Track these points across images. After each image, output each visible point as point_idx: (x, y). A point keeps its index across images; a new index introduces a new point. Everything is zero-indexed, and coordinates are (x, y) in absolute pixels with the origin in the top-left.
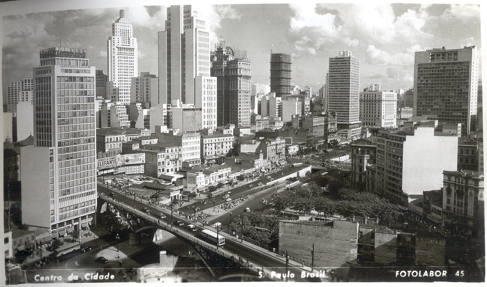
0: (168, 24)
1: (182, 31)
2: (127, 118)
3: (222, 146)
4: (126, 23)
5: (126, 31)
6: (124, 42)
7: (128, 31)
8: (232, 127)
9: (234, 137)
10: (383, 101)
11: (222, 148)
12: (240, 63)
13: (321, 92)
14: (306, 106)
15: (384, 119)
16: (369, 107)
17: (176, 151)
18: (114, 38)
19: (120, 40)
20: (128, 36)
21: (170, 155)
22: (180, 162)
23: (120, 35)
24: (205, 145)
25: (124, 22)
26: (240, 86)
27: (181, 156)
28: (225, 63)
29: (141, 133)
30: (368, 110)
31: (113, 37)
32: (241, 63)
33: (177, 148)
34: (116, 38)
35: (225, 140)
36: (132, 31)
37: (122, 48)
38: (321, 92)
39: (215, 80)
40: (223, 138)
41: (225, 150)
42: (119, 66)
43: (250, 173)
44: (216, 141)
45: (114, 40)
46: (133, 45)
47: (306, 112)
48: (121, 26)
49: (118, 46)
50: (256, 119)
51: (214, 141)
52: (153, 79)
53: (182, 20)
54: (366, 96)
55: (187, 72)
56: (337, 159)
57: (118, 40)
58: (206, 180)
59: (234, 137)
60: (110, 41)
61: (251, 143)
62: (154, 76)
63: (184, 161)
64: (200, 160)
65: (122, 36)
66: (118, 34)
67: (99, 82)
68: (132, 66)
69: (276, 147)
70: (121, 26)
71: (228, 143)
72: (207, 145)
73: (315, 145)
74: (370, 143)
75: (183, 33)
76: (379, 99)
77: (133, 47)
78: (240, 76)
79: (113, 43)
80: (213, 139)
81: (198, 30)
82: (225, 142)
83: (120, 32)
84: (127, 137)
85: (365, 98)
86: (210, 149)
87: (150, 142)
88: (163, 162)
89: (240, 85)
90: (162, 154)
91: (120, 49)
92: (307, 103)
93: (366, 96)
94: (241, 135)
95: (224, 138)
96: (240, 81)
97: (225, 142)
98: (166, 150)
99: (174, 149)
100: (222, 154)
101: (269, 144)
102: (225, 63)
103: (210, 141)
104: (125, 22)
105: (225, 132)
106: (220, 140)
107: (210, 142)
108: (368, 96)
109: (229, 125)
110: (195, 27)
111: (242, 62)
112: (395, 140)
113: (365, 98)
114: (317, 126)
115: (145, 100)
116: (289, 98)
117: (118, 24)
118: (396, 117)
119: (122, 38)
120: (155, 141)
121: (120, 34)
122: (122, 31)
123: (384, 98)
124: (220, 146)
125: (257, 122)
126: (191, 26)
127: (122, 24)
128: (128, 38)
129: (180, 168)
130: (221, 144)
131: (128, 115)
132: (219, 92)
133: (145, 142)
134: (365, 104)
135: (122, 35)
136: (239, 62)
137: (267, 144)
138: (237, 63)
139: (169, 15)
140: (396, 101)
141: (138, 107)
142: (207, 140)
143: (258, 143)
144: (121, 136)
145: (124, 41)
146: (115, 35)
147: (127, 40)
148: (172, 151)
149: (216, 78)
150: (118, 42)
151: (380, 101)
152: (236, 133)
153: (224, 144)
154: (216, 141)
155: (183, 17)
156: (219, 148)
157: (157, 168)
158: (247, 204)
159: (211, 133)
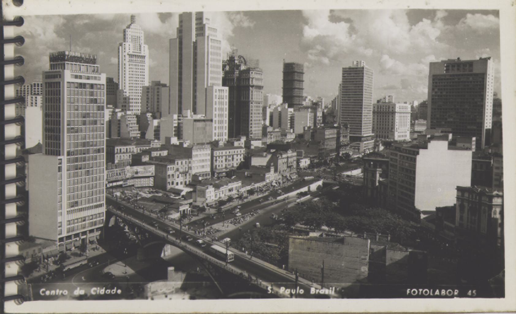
0: (180, 31)
1: (194, 39)
3: (233, 159)
6: (135, 49)
7: (140, 37)
8: (243, 139)
10: (396, 114)
12: (252, 73)
14: (318, 117)
16: (382, 119)
17: (186, 163)
18: (125, 45)
20: (140, 43)
21: (180, 168)
28: (237, 72)
30: (382, 122)
31: (124, 43)
32: (254, 72)
33: (187, 161)
34: (127, 44)
39: (226, 90)
47: (318, 124)
49: (129, 53)
51: (224, 154)
52: (163, 89)
55: (199, 82)
56: (349, 173)
60: (120, 47)
61: (262, 156)
62: (165, 86)
64: (210, 173)
68: (143, 74)
71: (239, 156)
74: (383, 156)
76: (393, 110)
78: (252, 86)
79: (124, 50)
80: (224, 152)
81: (210, 37)
83: (131, 38)
85: (378, 110)
90: (172, 166)
91: (131, 56)
92: (319, 114)
96: (252, 91)
98: (176, 162)
99: (184, 162)
101: (280, 157)
102: (237, 73)
105: (236, 144)
107: (221, 154)
110: (207, 34)
113: (378, 110)
119: (133, 45)
121: (131, 41)
123: (397, 110)
124: (231, 158)
127: (133, 30)
128: (140, 45)
129: (189, 181)
130: (232, 156)
131: (138, 126)
133: (155, 154)
134: (378, 116)
136: (251, 72)
137: (279, 157)
138: (249, 73)
139: (181, 22)
140: (410, 114)
143: (269, 156)
150: (129, 49)
151: (394, 113)
152: (248, 145)
153: (235, 156)
156: (229, 161)
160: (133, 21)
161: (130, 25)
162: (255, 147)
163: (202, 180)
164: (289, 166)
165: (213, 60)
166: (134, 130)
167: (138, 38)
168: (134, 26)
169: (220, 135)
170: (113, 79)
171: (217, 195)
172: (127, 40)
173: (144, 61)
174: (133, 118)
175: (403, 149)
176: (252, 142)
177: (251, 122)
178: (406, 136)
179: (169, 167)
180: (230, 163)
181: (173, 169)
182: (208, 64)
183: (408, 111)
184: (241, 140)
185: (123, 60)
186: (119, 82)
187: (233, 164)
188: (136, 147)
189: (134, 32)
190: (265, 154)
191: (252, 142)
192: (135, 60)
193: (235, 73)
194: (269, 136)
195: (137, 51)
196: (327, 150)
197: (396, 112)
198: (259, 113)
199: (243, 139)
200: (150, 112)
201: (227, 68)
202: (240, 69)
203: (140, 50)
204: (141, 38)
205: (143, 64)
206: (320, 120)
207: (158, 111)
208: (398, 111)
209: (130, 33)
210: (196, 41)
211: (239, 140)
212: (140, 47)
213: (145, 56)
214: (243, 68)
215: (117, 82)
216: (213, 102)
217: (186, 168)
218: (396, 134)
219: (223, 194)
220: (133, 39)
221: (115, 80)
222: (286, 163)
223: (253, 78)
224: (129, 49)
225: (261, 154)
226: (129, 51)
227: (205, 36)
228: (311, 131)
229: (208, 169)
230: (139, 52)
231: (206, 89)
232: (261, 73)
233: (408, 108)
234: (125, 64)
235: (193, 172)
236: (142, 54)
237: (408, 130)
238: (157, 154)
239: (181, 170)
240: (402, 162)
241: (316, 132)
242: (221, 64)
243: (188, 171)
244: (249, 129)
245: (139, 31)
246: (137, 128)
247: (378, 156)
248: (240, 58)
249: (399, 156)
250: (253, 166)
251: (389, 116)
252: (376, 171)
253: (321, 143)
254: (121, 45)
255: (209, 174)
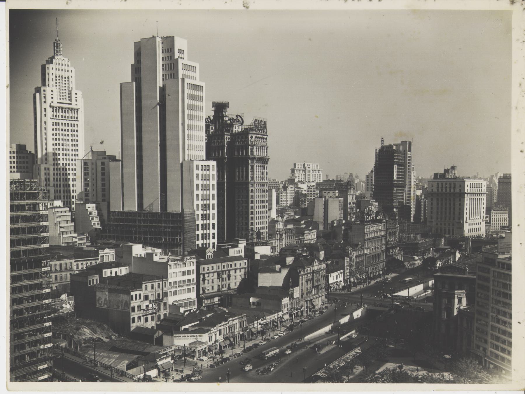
0: (137, 70)
1: (160, 83)
2: (73, 229)
3: (229, 276)
4: (65, 65)
5: (65, 78)
6: (61, 97)
7: (68, 78)
8: (242, 245)
9: (246, 261)
10: (466, 195)
11: (229, 279)
12: (252, 137)
13: (370, 179)
14: (350, 204)
15: (468, 224)
17: (159, 287)
18: (44, 91)
19: (55, 93)
20: (69, 87)
21: (150, 295)
22: (165, 304)
23: (54, 86)
24: (202, 276)
25: (60, 62)
26: (251, 174)
27: (167, 296)
28: (227, 136)
29: (100, 255)
31: (43, 88)
32: (254, 136)
33: (161, 283)
34: (48, 89)
35: (233, 267)
36: (74, 79)
37: (59, 108)
38: (370, 179)
39: (213, 166)
40: (230, 263)
41: (235, 281)
42: (53, 139)
43: (274, 319)
44: (219, 268)
45: (44, 93)
46: (76, 103)
47: (350, 214)
48: (56, 69)
49: (52, 104)
50: (276, 228)
51: (215, 269)
52: (112, 164)
53: (159, 63)
54: (440, 186)
55: (169, 154)
56: (404, 293)
57: (52, 93)
58: (211, 335)
59: (246, 261)
60: (38, 95)
61: (274, 271)
62: (113, 158)
63: (171, 304)
64: (196, 300)
65: (58, 87)
66: (51, 83)
67: (24, 165)
68: (76, 138)
69: (313, 276)
70: (56, 69)
71: (238, 271)
72: (206, 276)
73: (367, 269)
74: (462, 271)
75: (161, 86)
76: (460, 190)
77: (76, 107)
78: (253, 159)
79: (43, 100)
80: (215, 266)
81: (187, 81)
82: (233, 270)
83: (54, 80)
84: (76, 263)
85: (438, 190)
86: (211, 281)
87: (116, 273)
88: (139, 307)
89: (252, 174)
90: (138, 293)
91: (55, 109)
92: (352, 199)
93: (440, 186)
94: (257, 257)
95: (231, 263)
96: (252, 167)
97: (233, 270)
98: (144, 285)
99: (156, 285)
100: (229, 288)
101: (302, 273)
102: (228, 137)
103: (210, 269)
104: (63, 63)
105: (232, 252)
106: (225, 267)
107: (211, 270)
108: (442, 185)
109: (238, 241)
110: (180, 76)
111: (255, 135)
112: (501, 273)
113: (438, 190)
114: (370, 239)
115: (100, 200)
116: (323, 192)
117: (51, 66)
118: (485, 219)
119: (58, 91)
120: (124, 271)
121: (55, 84)
122: (58, 78)
123: (467, 189)
124: (225, 276)
125: (277, 233)
126: (175, 75)
127: (57, 67)
128: (69, 90)
129: (165, 315)
130: (227, 272)
131: (73, 224)
132: (220, 185)
133: (107, 273)
134: (438, 199)
135: (58, 84)
136: (250, 136)
137: (300, 272)
138: (247, 138)
139: (138, 55)
140: (485, 195)
141: (89, 209)
142: (206, 267)
143: (285, 272)
144: (68, 261)
145: (61, 96)
146: (47, 84)
147: (67, 95)
148: (152, 288)
149: (215, 163)
150: (52, 98)
151: (462, 195)
152: (249, 253)
153: (232, 272)
154: (219, 268)
155: (161, 59)
156: (223, 280)
157: (129, 315)
158: (16, 260)
159: (211, 254)
160: (57, 52)
161: (53, 57)
162: (262, 256)
163: (185, 312)
164: (315, 285)
165: (191, 117)
166: (67, 232)
167: (67, 79)
168: (59, 59)
169: (205, 236)
170: (25, 146)
171: (211, 336)
172: (47, 83)
173: (77, 118)
174: (65, 211)
175: (499, 263)
176: (257, 249)
177: (252, 216)
178: (479, 229)
179: (133, 293)
180: (225, 283)
181: (140, 298)
182: (183, 124)
183: (483, 191)
184: (239, 245)
185: (43, 115)
186: (36, 151)
187: (229, 284)
188: (75, 261)
189: (59, 70)
190: (278, 267)
191: (257, 249)
192: (62, 117)
193: (226, 136)
194: (278, 237)
195: (64, 101)
196: (367, 256)
197: (465, 193)
198: (263, 202)
199: (242, 245)
200: (93, 202)
201: (212, 130)
202: (232, 130)
203: (70, 100)
204: (70, 80)
205: (76, 123)
206: (352, 209)
207: (104, 200)
208: (469, 191)
209: (54, 71)
210: (163, 85)
211: (237, 246)
212: (70, 93)
213: (78, 110)
214: (237, 129)
215: (33, 152)
216: (193, 186)
217: (159, 295)
218: (466, 227)
219: (220, 335)
220: (58, 81)
221: (30, 148)
222: (310, 281)
223: (253, 146)
224: (52, 98)
225: (271, 267)
226: (52, 100)
227: (178, 78)
228: (343, 227)
229: (193, 295)
230: (69, 102)
231: (182, 164)
232: (265, 137)
233: (483, 186)
234: (45, 122)
235: (171, 300)
236: (73, 106)
237: (483, 221)
238: (111, 273)
239: (151, 298)
240: (498, 282)
241: (351, 228)
242: (204, 124)
243: (162, 299)
244: (249, 226)
245: (66, 68)
246: (72, 229)
247: (456, 270)
248: (238, 117)
249: (492, 273)
250: (261, 287)
251: (454, 200)
252: (454, 294)
253: (359, 246)
254: (38, 90)
255: (194, 301)
